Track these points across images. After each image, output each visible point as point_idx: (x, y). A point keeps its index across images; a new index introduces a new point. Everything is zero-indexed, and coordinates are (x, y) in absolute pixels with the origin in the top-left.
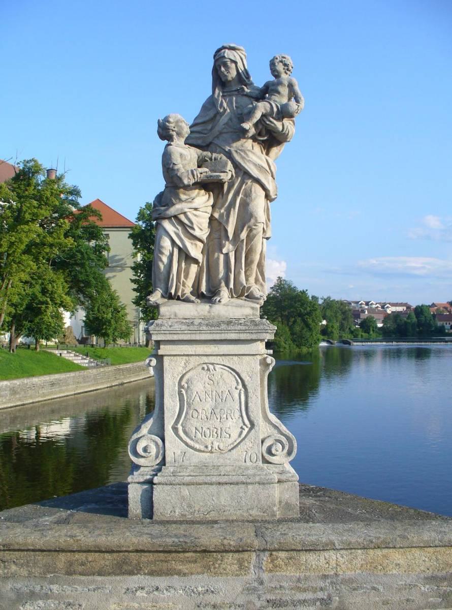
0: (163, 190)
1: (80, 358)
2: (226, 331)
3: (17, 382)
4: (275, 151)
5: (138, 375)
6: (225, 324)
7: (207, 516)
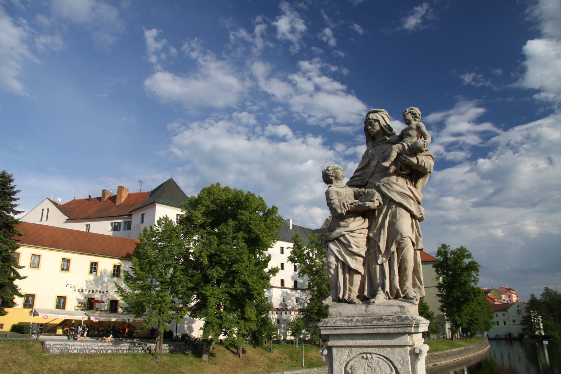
2: (377, 327)
4: (420, 182)
5: (446, 360)
6: (376, 320)
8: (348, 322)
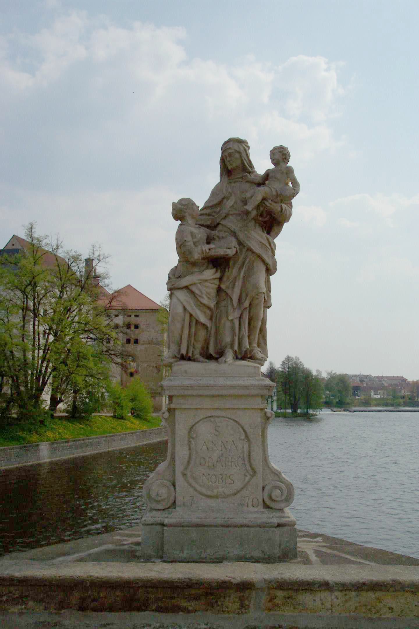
0: (176, 265)
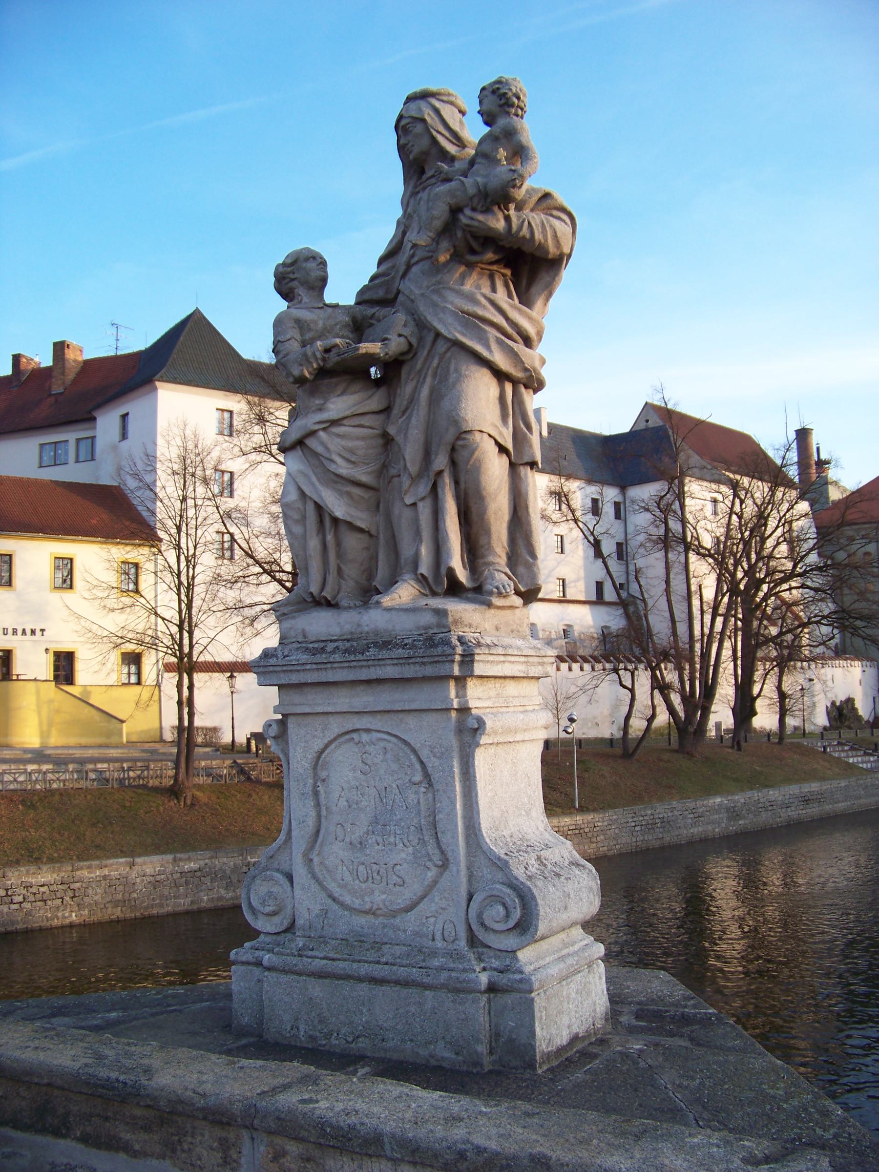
1: (862, 752)
3: (740, 798)
7: (353, 1045)
8: (314, 655)
